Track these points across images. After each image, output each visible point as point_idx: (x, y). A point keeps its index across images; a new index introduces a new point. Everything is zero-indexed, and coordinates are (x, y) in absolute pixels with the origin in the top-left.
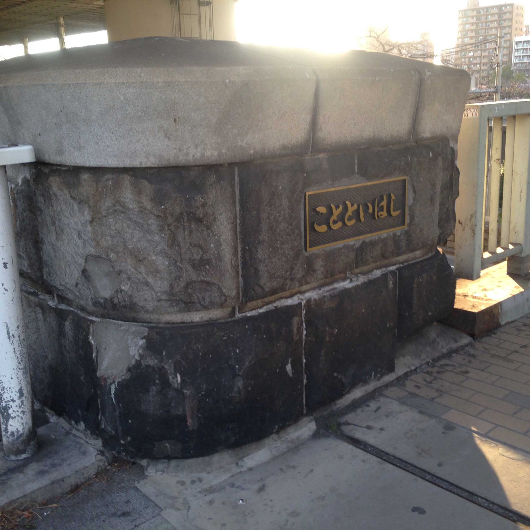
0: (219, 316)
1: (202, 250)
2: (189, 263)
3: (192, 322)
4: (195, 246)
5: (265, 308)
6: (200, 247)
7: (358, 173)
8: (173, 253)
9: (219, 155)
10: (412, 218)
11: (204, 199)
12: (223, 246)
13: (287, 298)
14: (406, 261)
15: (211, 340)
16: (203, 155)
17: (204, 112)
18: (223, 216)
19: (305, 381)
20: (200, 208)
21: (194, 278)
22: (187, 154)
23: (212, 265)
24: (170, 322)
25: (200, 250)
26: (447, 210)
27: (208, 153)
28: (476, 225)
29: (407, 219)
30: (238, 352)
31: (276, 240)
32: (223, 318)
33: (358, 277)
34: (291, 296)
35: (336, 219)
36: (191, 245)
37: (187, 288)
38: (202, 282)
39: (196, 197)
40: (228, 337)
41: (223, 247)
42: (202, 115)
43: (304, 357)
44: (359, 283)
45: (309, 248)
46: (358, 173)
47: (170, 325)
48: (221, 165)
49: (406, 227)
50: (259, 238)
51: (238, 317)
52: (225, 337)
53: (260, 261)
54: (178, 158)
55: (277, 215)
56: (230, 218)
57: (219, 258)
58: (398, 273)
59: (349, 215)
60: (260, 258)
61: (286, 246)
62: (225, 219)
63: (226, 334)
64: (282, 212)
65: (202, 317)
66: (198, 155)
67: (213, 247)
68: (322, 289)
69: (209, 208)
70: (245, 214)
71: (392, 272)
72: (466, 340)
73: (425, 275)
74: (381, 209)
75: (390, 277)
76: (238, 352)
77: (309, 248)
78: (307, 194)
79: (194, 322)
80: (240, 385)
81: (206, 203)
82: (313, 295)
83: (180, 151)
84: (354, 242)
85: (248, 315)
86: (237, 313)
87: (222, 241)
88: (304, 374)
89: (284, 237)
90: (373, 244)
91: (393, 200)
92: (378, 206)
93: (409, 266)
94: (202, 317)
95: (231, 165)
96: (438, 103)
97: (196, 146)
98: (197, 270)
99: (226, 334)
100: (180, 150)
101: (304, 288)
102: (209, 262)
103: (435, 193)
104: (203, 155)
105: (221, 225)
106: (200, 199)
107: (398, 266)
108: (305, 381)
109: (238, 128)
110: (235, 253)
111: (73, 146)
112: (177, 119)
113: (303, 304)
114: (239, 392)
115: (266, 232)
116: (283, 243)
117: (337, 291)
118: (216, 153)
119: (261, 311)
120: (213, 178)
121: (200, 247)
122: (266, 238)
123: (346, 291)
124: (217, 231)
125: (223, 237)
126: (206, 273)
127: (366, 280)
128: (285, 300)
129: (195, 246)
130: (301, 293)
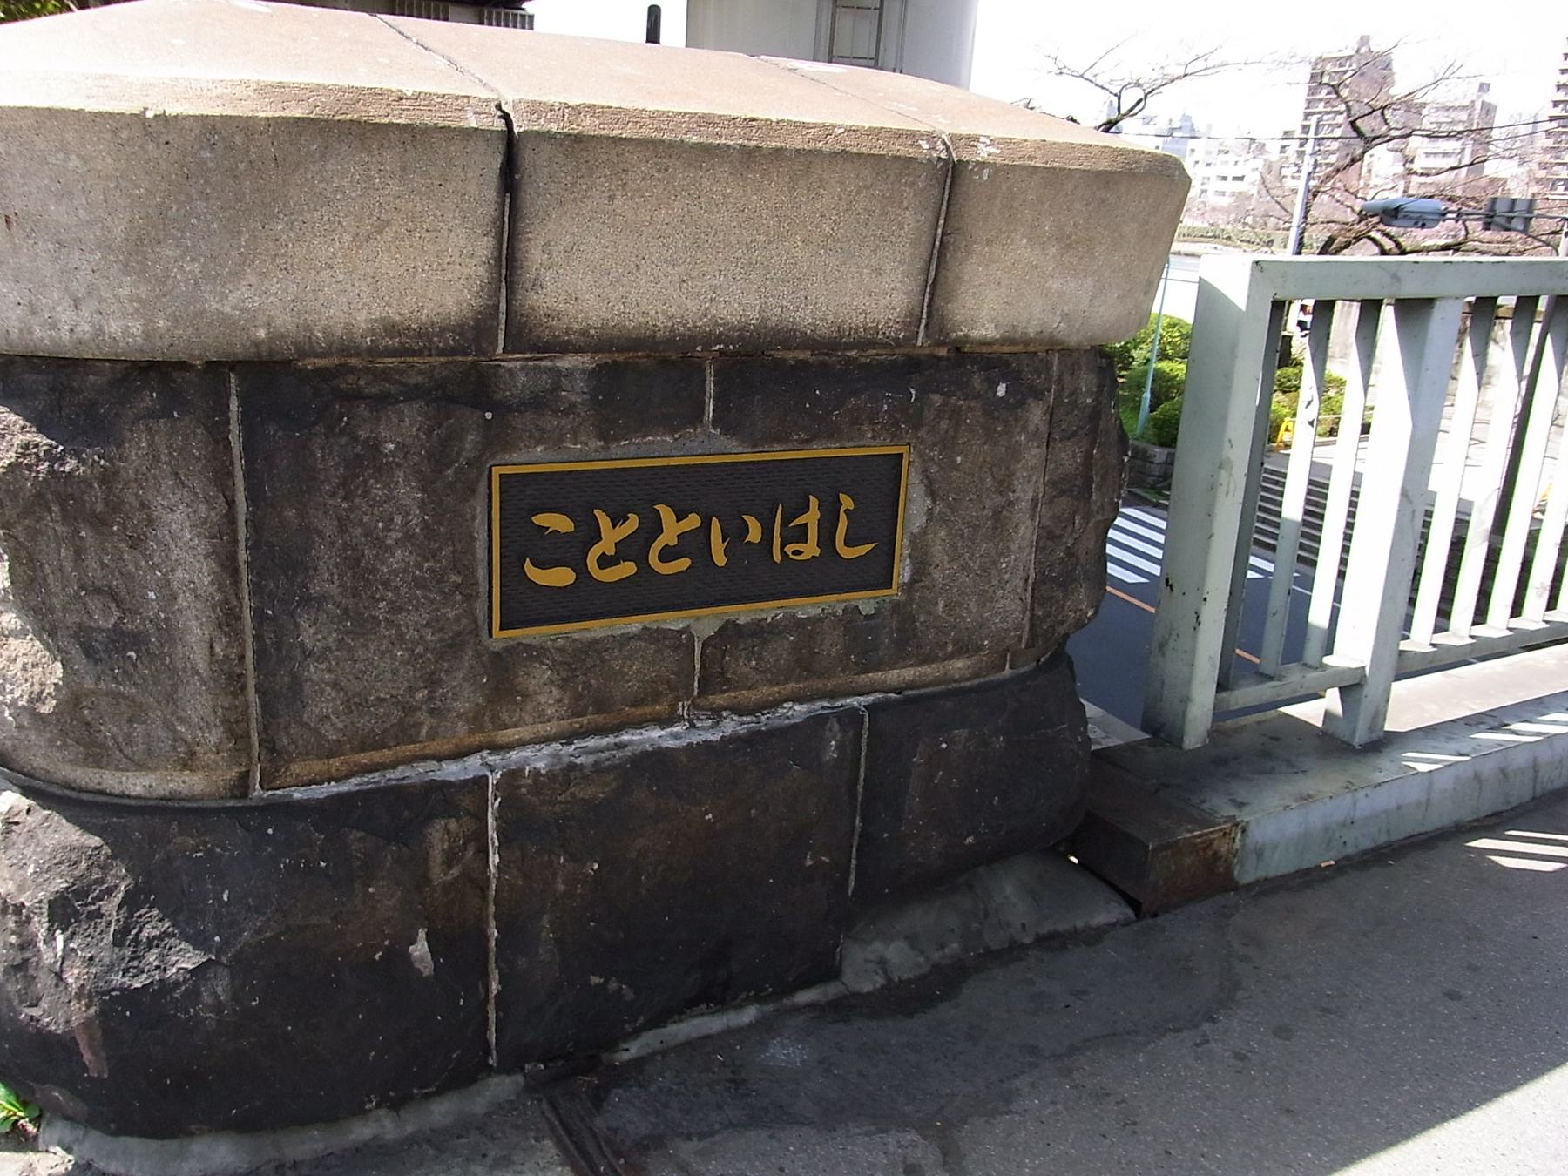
0: (198, 789)
1: (118, 606)
2: (76, 636)
3: (123, 796)
4: (97, 591)
5: (354, 780)
6: (113, 596)
7: (715, 423)
8: (32, 604)
9: (147, 335)
10: (921, 567)
11: (111, 460)
12: (180, 600)
13: (440, 758)
14: (912, 685)
15: (157, 856)
16: (99, 332)
17: (84, 201)
18: (180, 514)
19: (495, 987)
20: (96, 485)
21: (89, 684)
22: (54, 326)
23: (147, 650)
24: (73, 785)
25: (113, 606)
26: (1070, 553)
27: (114, 327)
28: (1205, 599)
29: (903, 571)
30: (226, 899)
31: (373, 598)
32: (211, 796)
33: (721, 716)
34: (459, 755)
35: (611, 552)
36: (82, 588)
37: (76, 705)
38: (110, 693)
39: (85, 451)
40: (209, 852)
41: (182, 602)
42: (81, 212)
43: (493, 923)
44: (714, 737)
45: (501, 629)
46: (715, 423)
47: (68, 792)
48: (182, 365)
49: (893, 593)
50: (307, 589)
51: (261, 798)
52: (199, 851)
53: (307, 654)
54: (30, 332)
55: (376, 527)
56: (205, 523)
57: (169, 633)
58: (867, 720)
59: (604, 554)
60: (309, 644)
61: (409, 619)
62: (188, 524)
63: (205, 844)
64: (398, 519)
65: (151, 786)
66: (85, 329)
67: (152, 600)
68: (578, 743)
69: (126, 485)
70: (259, 513)
71: (850, 718)
72: (1107, 912)
73: (961, 733)
74: (801, 534)
75: (832, 727)
76: (226, 899)
77: (501, 629)
78: (497, 471)
79: (129, 797)
80: (219, 989)
81: (116, 473)
82: (538, 759)
83: (34, 312)
84: (705, 622)
85: (297, 796)
86: (258, 786)
87: (175, 585)
88: (492, 965)
89: (403, 591)
90: (761, 631)
91: (847, 511)
92: (784, 524)
93: (909, 701)
94: (151, 786)
95: (217, 369)
96: (1025, 240)
97: (77, 303)
98: (97, 662)
99: (205, 844)
100: (34, 312)
101: (511, 735)
102: (137, 640)
103: (1011, 503)
104: (99, 332)
105: (172, 538)
106: (96, 457)
107: (870, 698)
108: (495, 987)
109: (202, 260)
110: (228, 620)
111: (1342, 324)
112: (12, 217)
113: (492, 780)
114: (218, 1007)
115: (332, 574)
116: (395, 608)
117: (628, 752)
118: (136, 328)
119: (344, 788)
120: (149, 399)
121: (113, 596)
122: (334, 589)
123: (659, 757)
124: (160, 557)
125: (179, 572)
126: (125, 672)
127: (742, 730)
128: (433, 764)
129: (97, 591)
130: (495, 748)
